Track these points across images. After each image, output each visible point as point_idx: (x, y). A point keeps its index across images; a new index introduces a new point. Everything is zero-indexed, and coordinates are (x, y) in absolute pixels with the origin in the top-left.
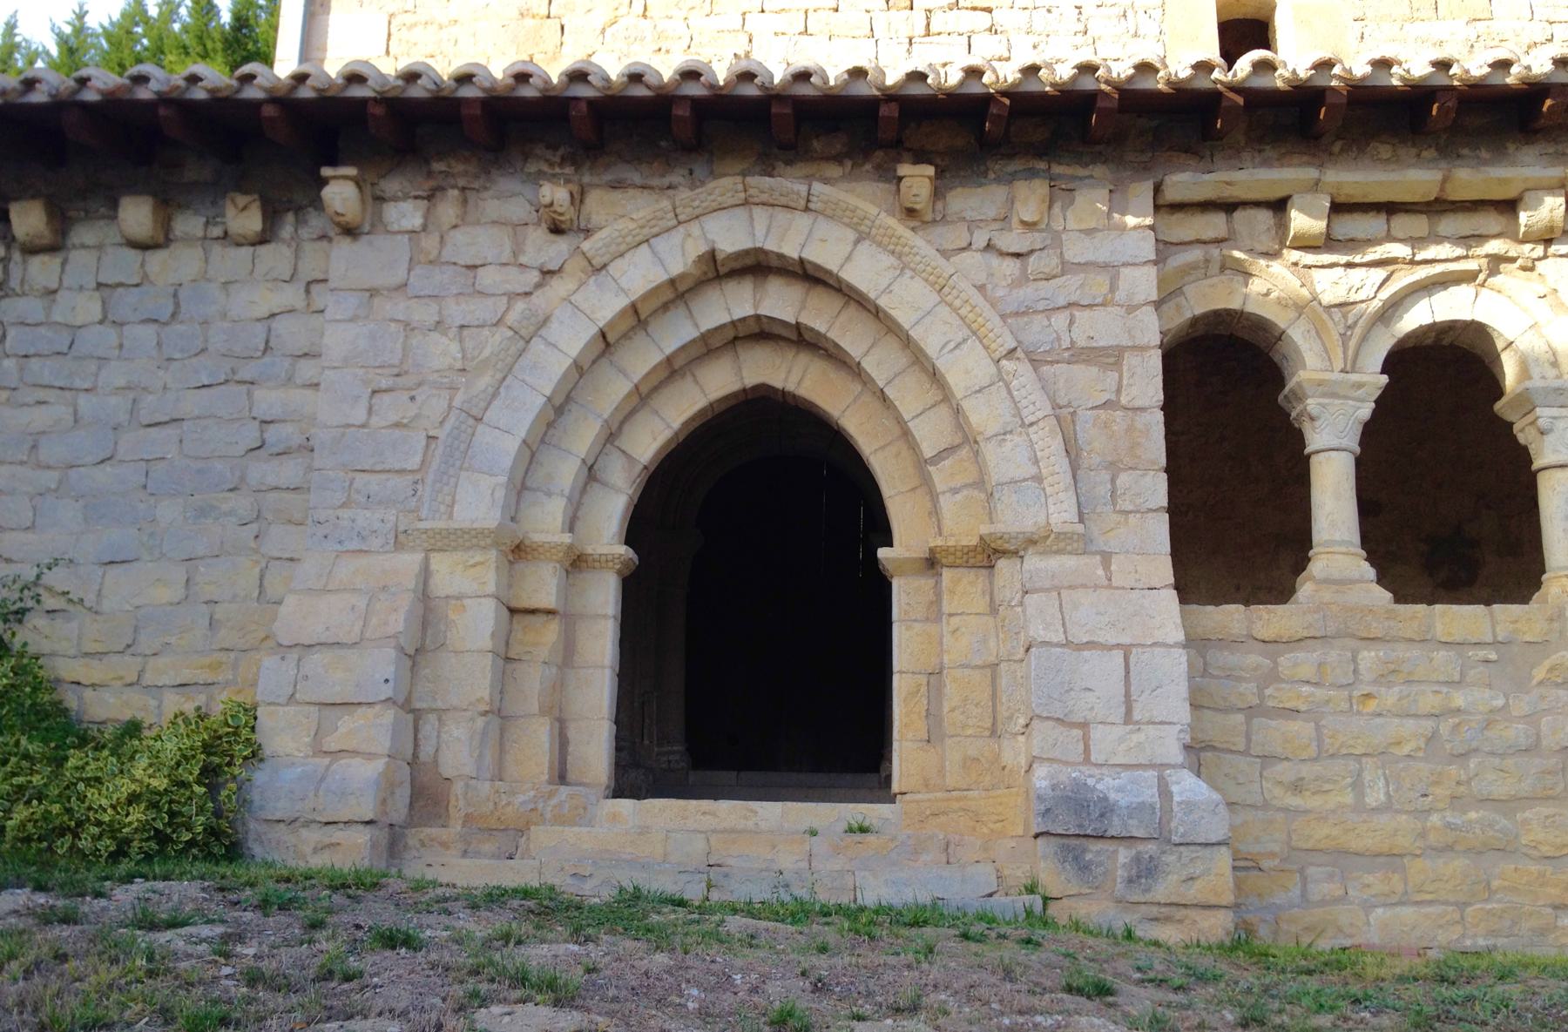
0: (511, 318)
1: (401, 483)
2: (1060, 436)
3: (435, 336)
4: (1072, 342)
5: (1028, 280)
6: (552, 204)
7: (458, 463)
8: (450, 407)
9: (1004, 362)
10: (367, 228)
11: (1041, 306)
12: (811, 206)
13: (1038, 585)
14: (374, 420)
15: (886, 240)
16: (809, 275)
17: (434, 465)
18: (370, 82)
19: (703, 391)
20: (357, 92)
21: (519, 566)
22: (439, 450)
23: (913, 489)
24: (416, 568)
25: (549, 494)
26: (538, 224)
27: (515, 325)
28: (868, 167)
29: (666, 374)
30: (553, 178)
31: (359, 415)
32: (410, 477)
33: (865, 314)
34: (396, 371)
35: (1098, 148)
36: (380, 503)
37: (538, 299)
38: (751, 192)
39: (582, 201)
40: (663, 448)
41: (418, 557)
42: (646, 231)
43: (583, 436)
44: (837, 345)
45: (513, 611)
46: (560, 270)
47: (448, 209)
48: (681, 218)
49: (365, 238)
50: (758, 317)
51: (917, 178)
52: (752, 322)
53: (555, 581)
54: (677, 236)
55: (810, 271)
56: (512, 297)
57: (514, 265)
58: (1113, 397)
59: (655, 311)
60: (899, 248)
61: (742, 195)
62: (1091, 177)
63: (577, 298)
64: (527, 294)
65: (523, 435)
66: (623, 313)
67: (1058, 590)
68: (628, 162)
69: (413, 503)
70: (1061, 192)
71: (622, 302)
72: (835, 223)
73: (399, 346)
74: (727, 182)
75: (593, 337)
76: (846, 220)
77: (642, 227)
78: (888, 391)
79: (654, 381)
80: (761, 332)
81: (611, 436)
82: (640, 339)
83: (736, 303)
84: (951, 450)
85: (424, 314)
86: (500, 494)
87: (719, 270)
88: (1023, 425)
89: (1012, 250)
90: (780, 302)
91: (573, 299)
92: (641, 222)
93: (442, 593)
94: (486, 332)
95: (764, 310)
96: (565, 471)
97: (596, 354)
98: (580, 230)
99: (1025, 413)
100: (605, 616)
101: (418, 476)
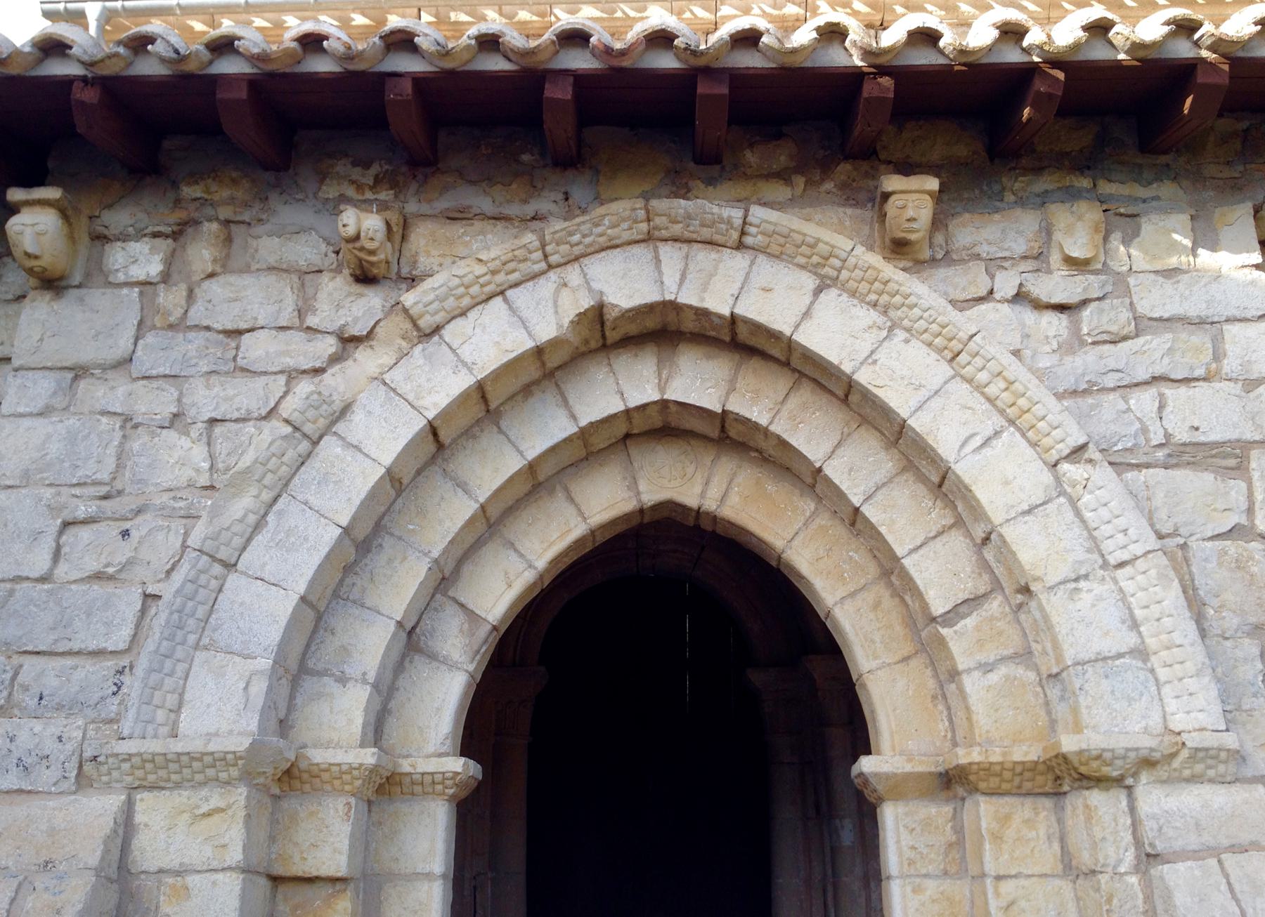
0: (290, 407)
1: (96, 673)
2: (1176, 583)
3: (170, 436)
4: (1167, 435)
5: (1083, 343)
6: (357, 237)
7: (192, 638)
8: (184, 547)
9: (1065, 467)
10: (77, 279)
11: (1110, 381)
12: (749, 240)
13: (1178, 845)
14: (62, 571)
15: (864, 287)
16: (741, 342)
17: (150, 645)
18: (75, 51)
19: (581, 513)
20: (58, 68)
21: (289, 804)
22: (160, 616)
23: (906, 659)
24: (106, 824)
25: (343, 680)
26: (338, 270)
27: (296, 417)
28: (829, 185)
29: (528, 487)
30: (363, 205)
31: (39, 561)
32: (111, 664)
33: (825, 398)
34: (103, 490)
35: (1163, 159)
36: (59, 707)
37: (336, 382)
38: (658, 221)
39: (404, 238)
40: (520, 598)
41: (114, 801)
42: (500, 278)
43: (399, 585)
44: (784, 444)
45: (276, 880)
46: (370, 335)
47: (201, 253)
48: (554, 259)
49: (74, 293)
50: (664, 404)
51: (912, 197)
52: (653, 412)
53: (347, 828)
54: (546, 286)
55: (743, 334)
56: (293, 375)
57: (300, 329)
58: (1243, 520)
59: (511, 398)
60: (885, 298)
61: (644, 227)
62: (1157, 198)
63: (395, 377)
64: (318, 371)
65: (301, 587)
66: (464, 397)
67: (1215, 852)
68: (473, 183)
69: (113, 707)
70: (1122, 220)
71: (461, 383)
72: (785, 268)
73: (112, 450)
74: (621, 207)
75: (422, 430)
76: (802, 260)
77: (494, 273)
78: (868, 511)
79: (509, 499)
80: (666, 426)
81: (444, 582)
82: (489, 439)
83: (634, 384)
84: (974, 602)
85: (154, 402)
86: (259, 688)
87: (608, 335)
88: (1105, 565)
89: (1056, 300)
90: (698, 382)
91: (387, 377)
92: (492, 266)
93: (152, 865)
94: (250, 428)
95: (676, 393)
96: (370, 642)
97: (423, 459)
98: (400, 278)
99: (1107, 546)
100: (429, 876)
101: (125, 661)
